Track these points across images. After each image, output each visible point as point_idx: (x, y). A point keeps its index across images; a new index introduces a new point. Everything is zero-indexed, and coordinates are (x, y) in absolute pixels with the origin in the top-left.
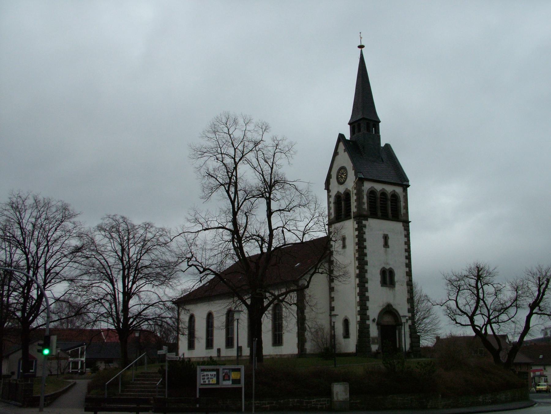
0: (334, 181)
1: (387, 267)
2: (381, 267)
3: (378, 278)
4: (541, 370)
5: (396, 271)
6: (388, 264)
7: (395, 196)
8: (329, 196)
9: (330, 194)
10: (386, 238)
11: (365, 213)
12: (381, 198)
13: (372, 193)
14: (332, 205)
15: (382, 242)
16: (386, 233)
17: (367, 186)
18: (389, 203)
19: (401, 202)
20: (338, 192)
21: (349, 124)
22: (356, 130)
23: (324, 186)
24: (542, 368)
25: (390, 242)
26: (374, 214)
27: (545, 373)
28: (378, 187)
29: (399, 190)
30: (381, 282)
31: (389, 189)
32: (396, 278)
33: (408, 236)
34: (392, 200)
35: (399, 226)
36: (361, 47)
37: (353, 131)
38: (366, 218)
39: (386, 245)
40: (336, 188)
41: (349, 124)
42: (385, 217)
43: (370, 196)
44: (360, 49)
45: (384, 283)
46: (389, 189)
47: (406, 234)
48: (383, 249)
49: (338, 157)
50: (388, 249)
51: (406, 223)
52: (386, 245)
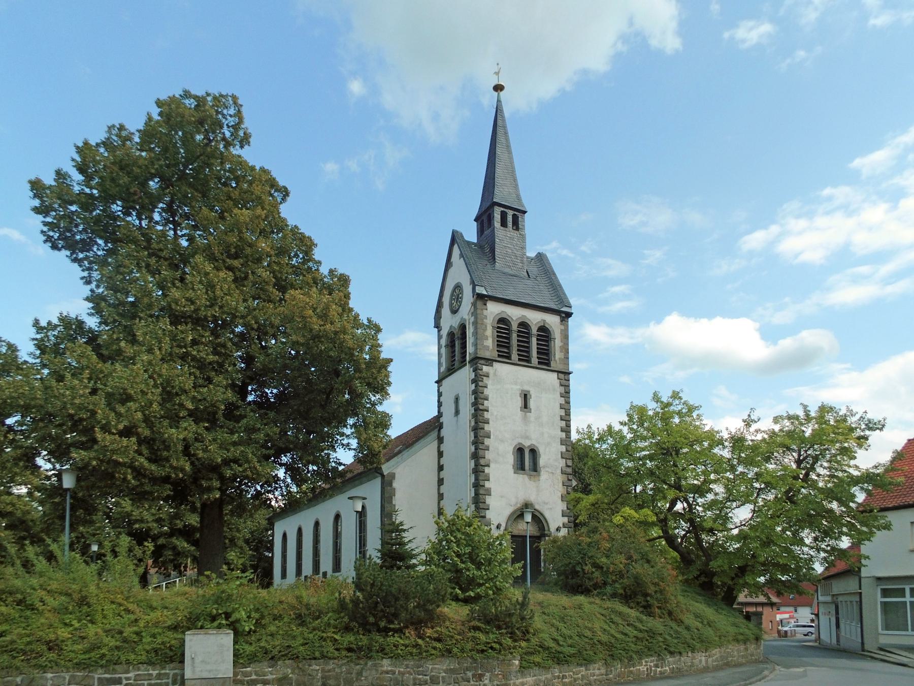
0: (446, 311)
1: (527, 443)
2: (515, 443)
3: (510, 459)
4: (792, 612)
5: (541, 450)
6: (527, 438)
7: (545, 333)
8: (440, 337)
9: (442, 332)
10: (526, 397)
11: (487, 355)
12: (519, 331)
13: (503, 321)
14: (443, 350)
15: (519, 402)
16: (526, 388)
17: (494, 310)
18: (534, 341)
19: (556, 340)
20: (451, 327)
21: (475, 220)
22: (486, 225)
23: (432, 322)
24: (792, 609)
25: (532, 403)
26: (504, 355)
27: (796, 615)
28: (515, 314)
29: (552, 321)
30: (513, 466)
31: (535, 318)
32: (542, 462)
33: (566, 394)
34: (538, 335)
35: (551, 378)
36: (498, 88)
37: (714, 454)
38: (489, 362)
39: (526, 406)
40: (449, 322)
41: (475, 220)
42: (525, 360)
43: (498, 327)
44: (496, 94)
45: (520, 467)
46: (535, 318)
47: (563, 391)
48: (519, 414)
49: (451, 271)
50: (528, 414)
51: (564, 374)
52: (526, 406)
